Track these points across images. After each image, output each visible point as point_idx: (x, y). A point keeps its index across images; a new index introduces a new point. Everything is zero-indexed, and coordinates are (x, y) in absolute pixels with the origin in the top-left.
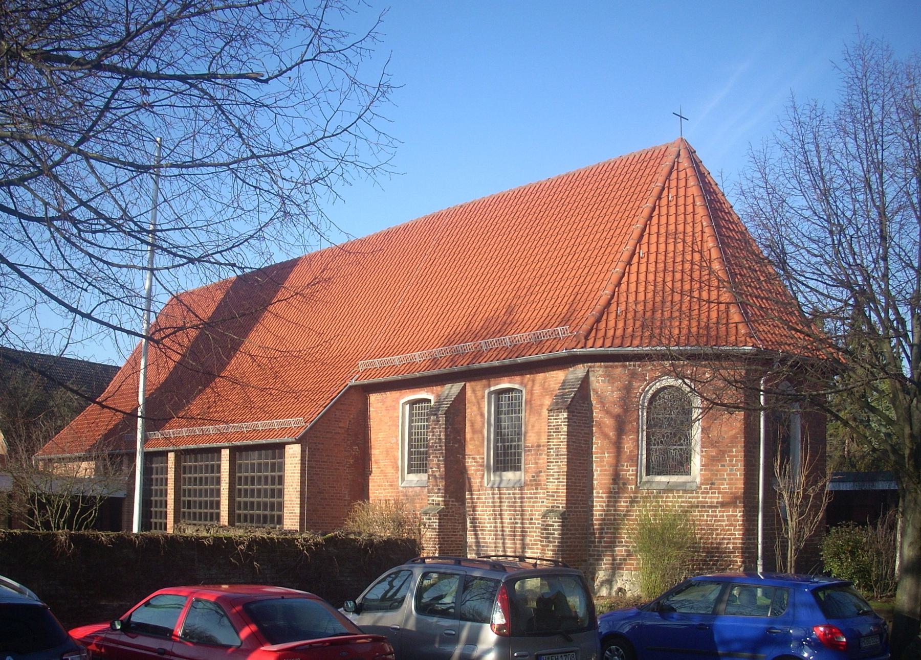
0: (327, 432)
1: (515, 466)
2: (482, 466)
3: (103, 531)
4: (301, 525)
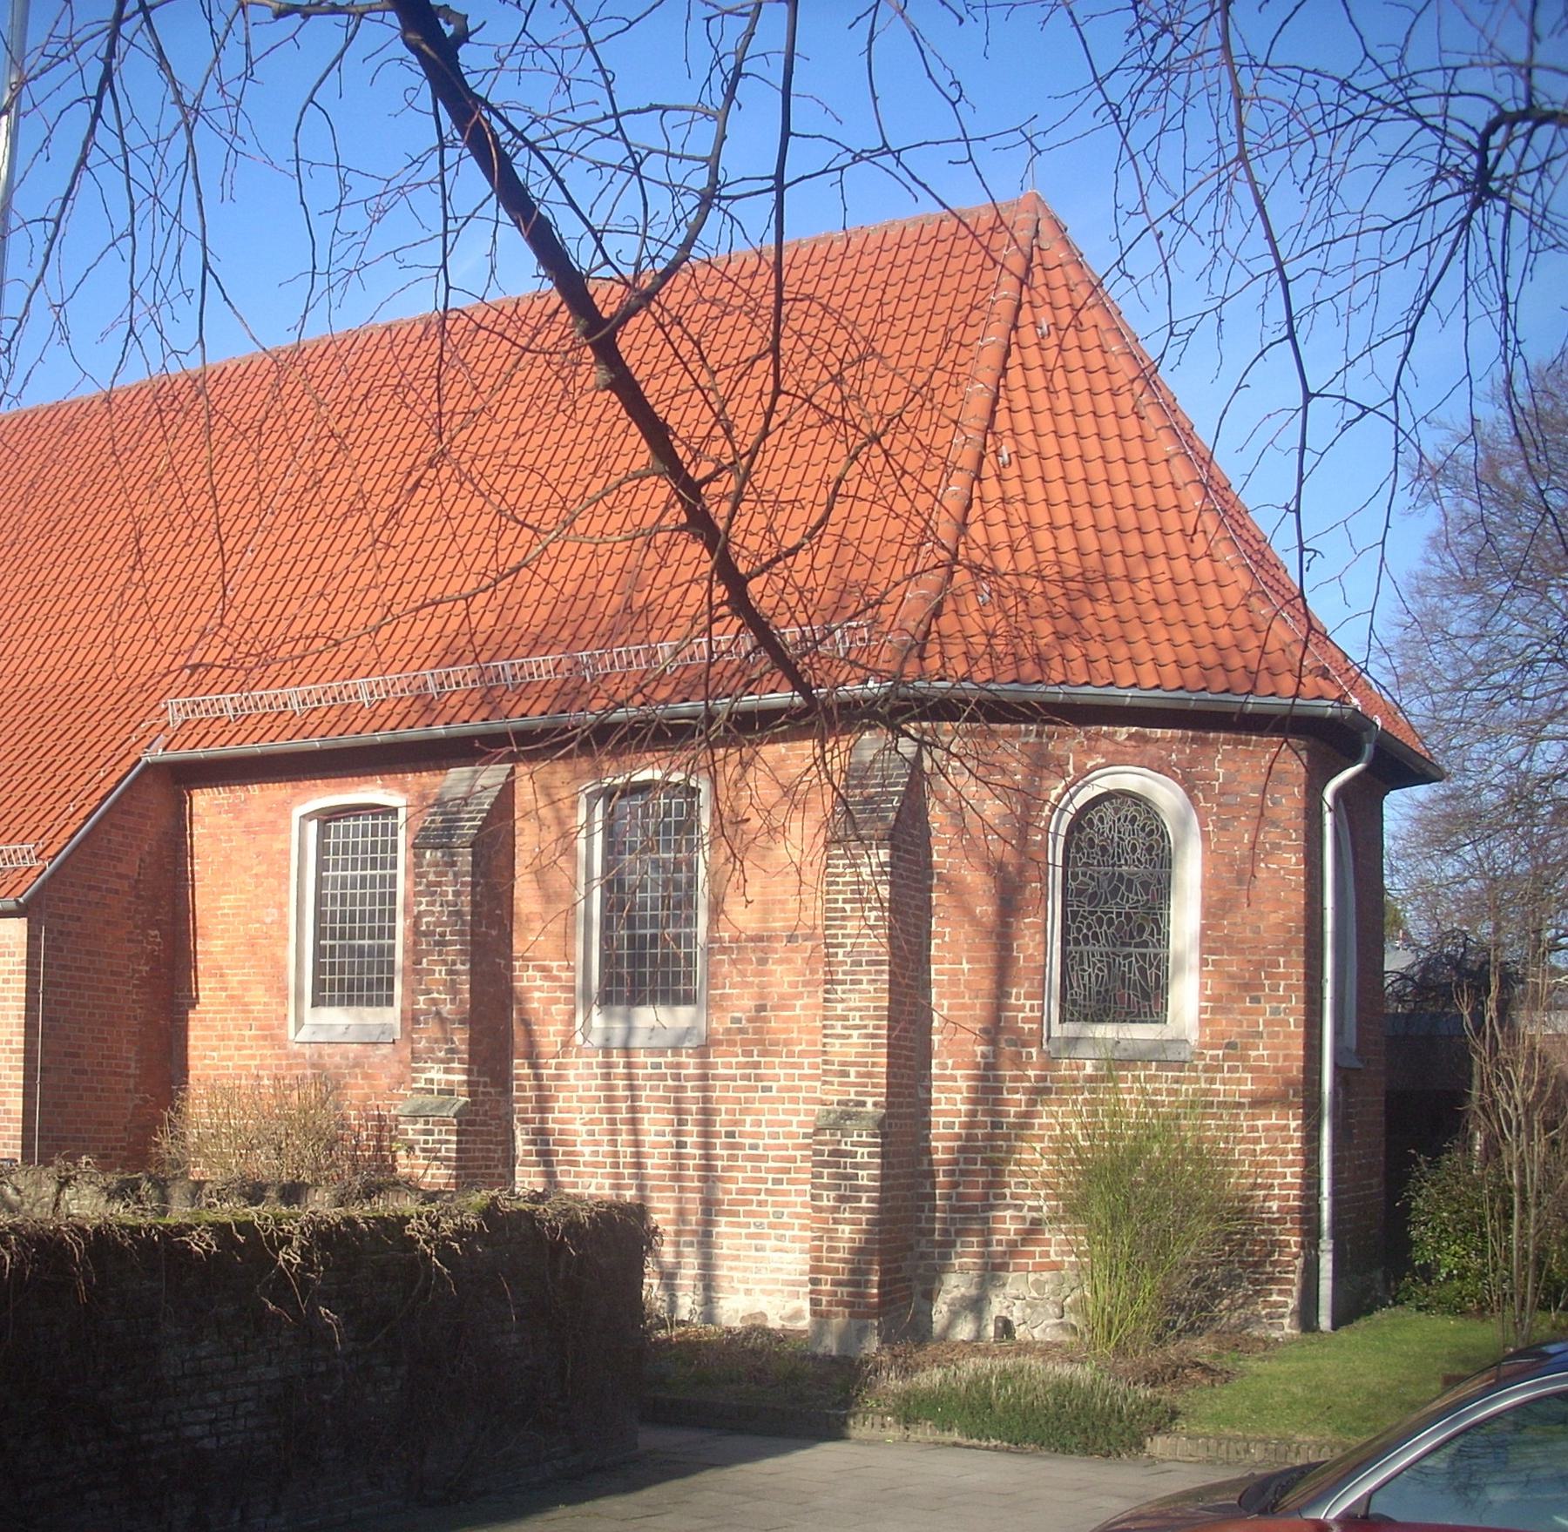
0: (91, 888)
1: (676, 993)
2: (572, 989)
3: (521, 1211)
4: (27, 1146)
